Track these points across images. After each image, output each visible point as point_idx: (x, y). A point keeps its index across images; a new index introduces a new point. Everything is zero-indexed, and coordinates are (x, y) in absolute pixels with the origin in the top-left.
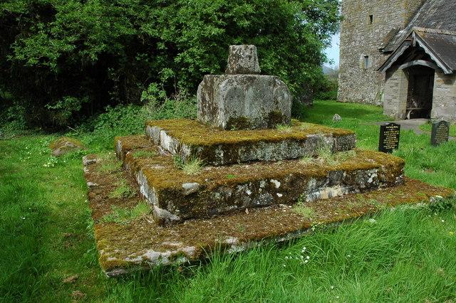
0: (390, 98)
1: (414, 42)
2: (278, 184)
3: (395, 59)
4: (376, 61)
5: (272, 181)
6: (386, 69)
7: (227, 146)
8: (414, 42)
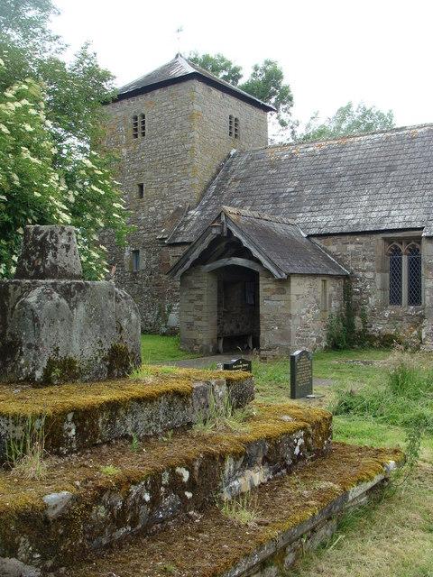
0: (190, 319)
1: (225, 229)
2: (186, 475)
3: (195, 255)
4: (153, 259)
5: (178, 470)
6: (181, 271)
7: (84, 416)
8: (225, 229)
